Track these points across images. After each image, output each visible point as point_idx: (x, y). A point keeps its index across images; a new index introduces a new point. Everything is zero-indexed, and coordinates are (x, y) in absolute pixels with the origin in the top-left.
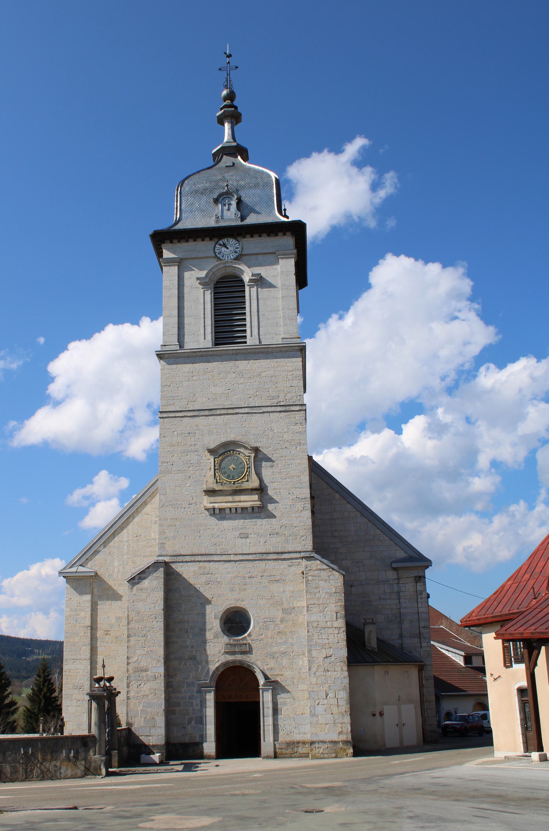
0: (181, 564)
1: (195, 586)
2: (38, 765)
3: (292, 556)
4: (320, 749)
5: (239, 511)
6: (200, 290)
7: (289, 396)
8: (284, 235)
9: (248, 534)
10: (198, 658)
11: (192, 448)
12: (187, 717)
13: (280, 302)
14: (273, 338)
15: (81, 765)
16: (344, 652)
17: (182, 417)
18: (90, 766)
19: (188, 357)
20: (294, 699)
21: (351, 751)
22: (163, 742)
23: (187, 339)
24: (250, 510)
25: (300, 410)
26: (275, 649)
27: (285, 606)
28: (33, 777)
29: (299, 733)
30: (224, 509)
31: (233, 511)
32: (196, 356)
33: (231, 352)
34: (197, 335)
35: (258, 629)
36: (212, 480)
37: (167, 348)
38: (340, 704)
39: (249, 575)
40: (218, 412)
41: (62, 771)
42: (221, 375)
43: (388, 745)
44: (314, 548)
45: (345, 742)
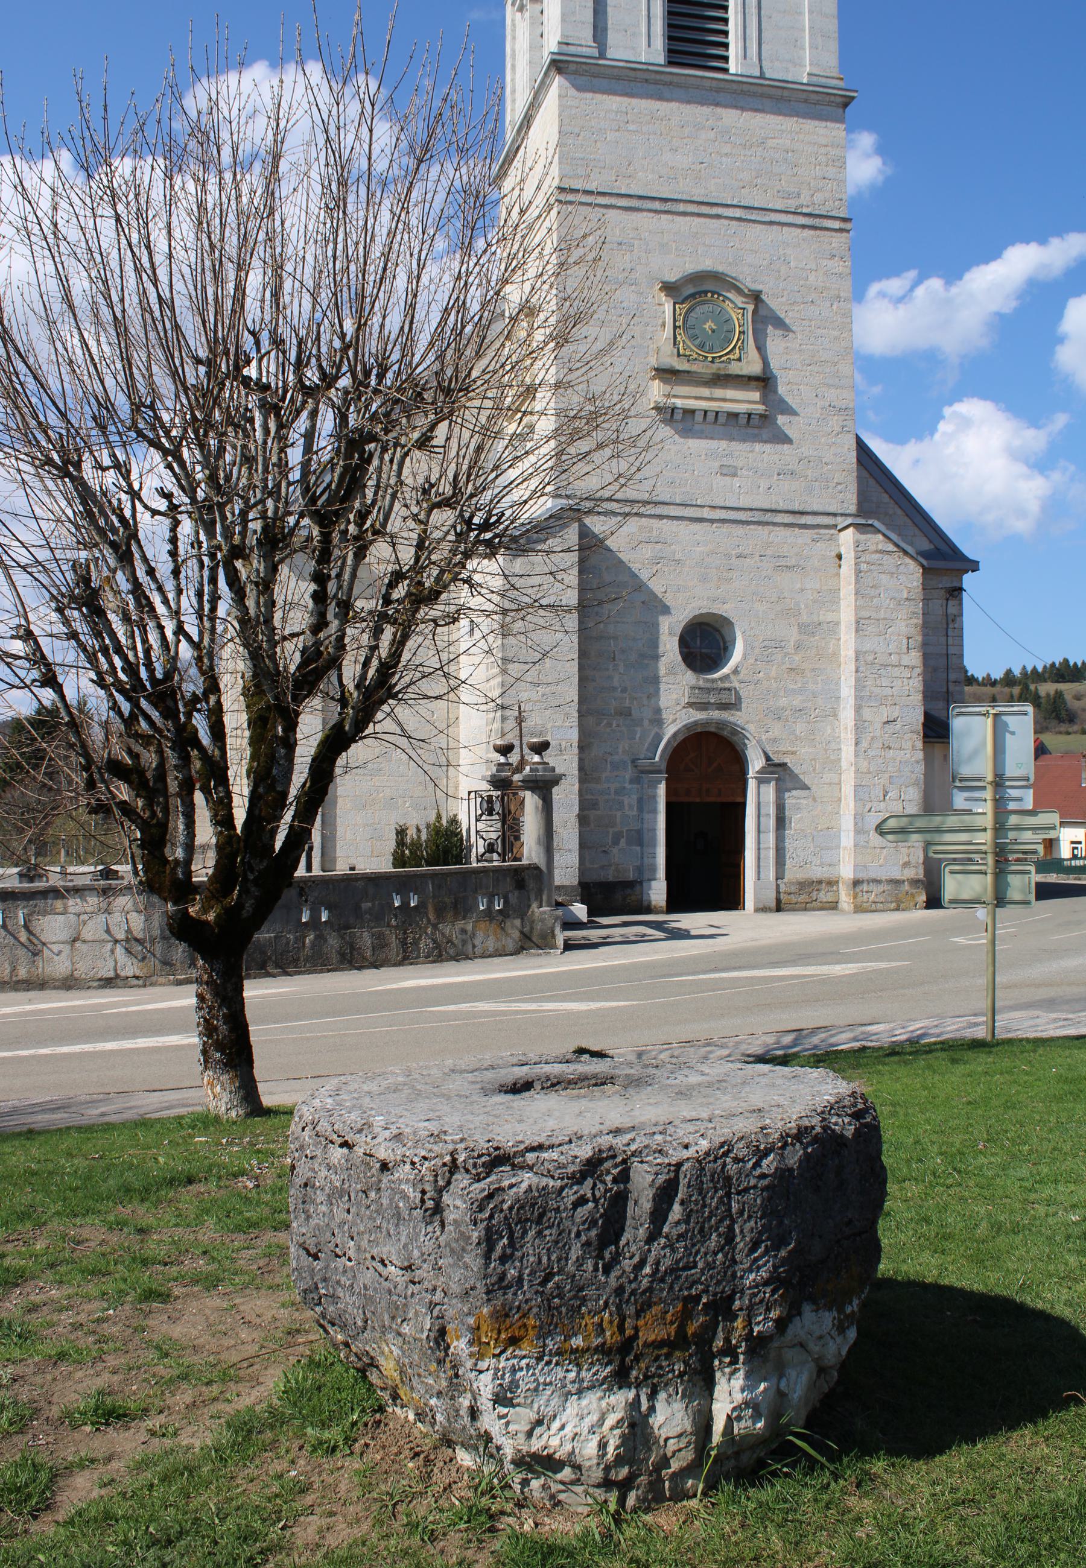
1: (631, 565)
2: (429, 930)
5: (722, 419)
7: (818, 197)
9: (736, 468)
12: (611, 830)
15: (514, 925)
17: (606, 206)
18: (532, 928)
19: (618, 78)
20: (814, 800)
21: (924, 898)
22: (576, 882)
23: (612, 38)
24: (743, 420)
25: (841, 230)
26: (783, 702)
27: (804, 618)
28: (418, 957)
29: (821, 865)
30: (693, 412)
31: (711, 417)
32: (635, 80)
33: (707, 84)
35: (752, 661)
36: (669, 348)
37: (572, 50)
40: (681, 207)
42: (687, 131)
45: (914, 882)
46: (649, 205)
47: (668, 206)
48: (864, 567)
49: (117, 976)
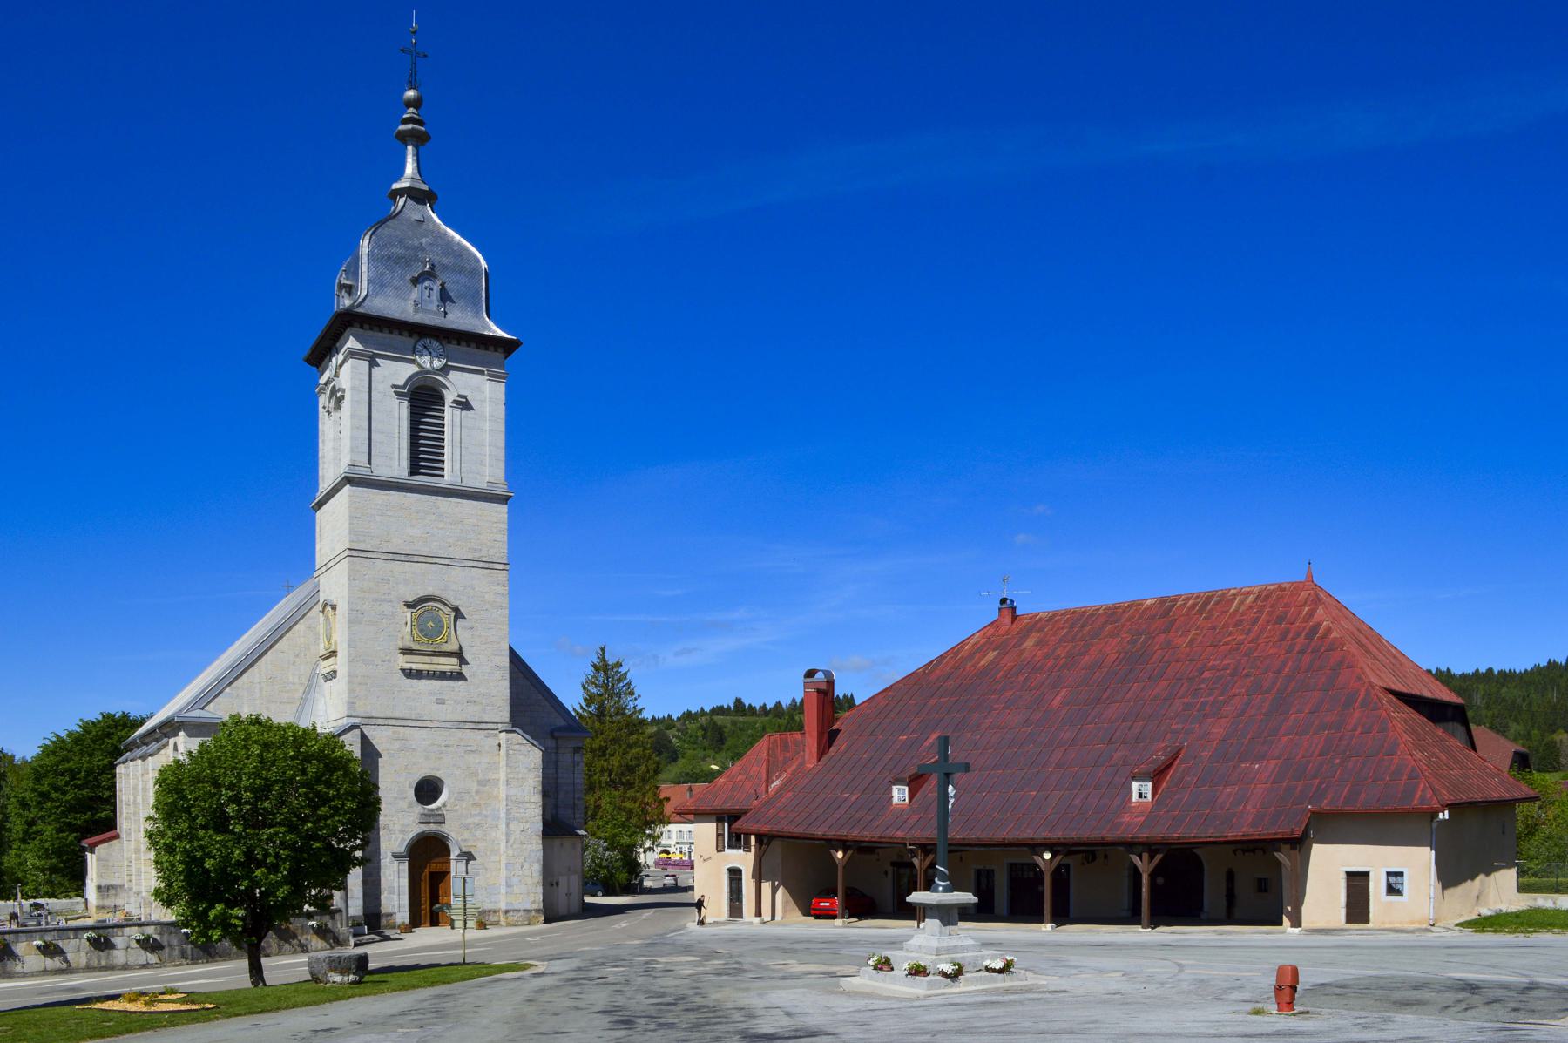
0: (373, 727)
4: (514, 917)
6: (395, 400)
8: (496, 351)
10: (391, 826)
11: (386, 597)
13: (487, 436)
16: (540, 827)
20: (486, 869)
21: (543, 918)
22: (361, 914)
26: (469, 820)
27: (480, 777)
29: (491, 902)
34: (391, 459)
36: (408, 637)
38: (534, 875)
40: (416, 559)
43: (561, 914)
45: (538, 911)
46: (398, 557)
47: (408, 558)
48: (511, 752)
49: (148, 963)
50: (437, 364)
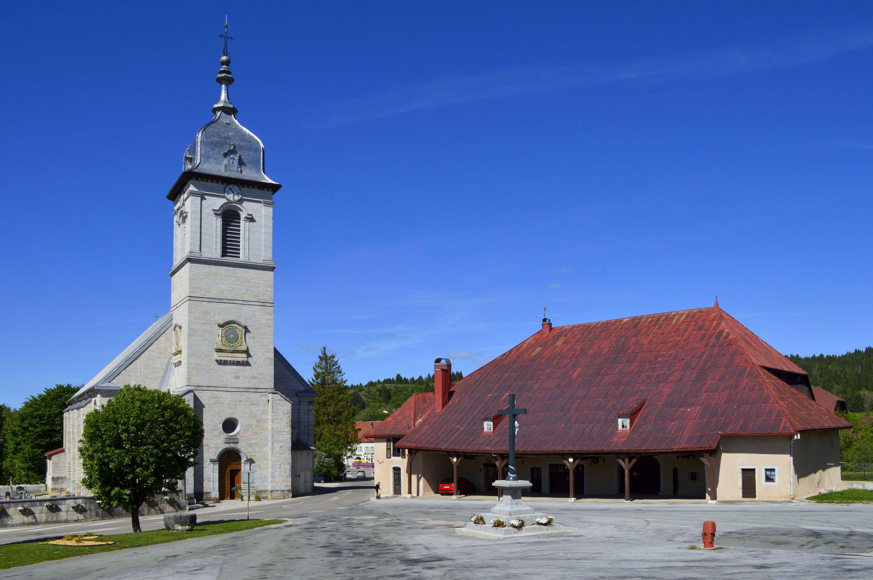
3: (263, 390)
4: (276, 494)
6: (214, 218)
8: (268, 190)
14: (257, 258)
16: (290, 445)
21: (291, 495)
22: (193, 492)
26: (252, 442)
27: (258, 418)
29: (263, 486)
36: (220, 343)
39: (239, 400)
40: (224, 301)
41: (166, 509)
44: (274, 387)
45: (288, 491)
46: (215, 300)
49: (78, 519)
50: (237, 198)
